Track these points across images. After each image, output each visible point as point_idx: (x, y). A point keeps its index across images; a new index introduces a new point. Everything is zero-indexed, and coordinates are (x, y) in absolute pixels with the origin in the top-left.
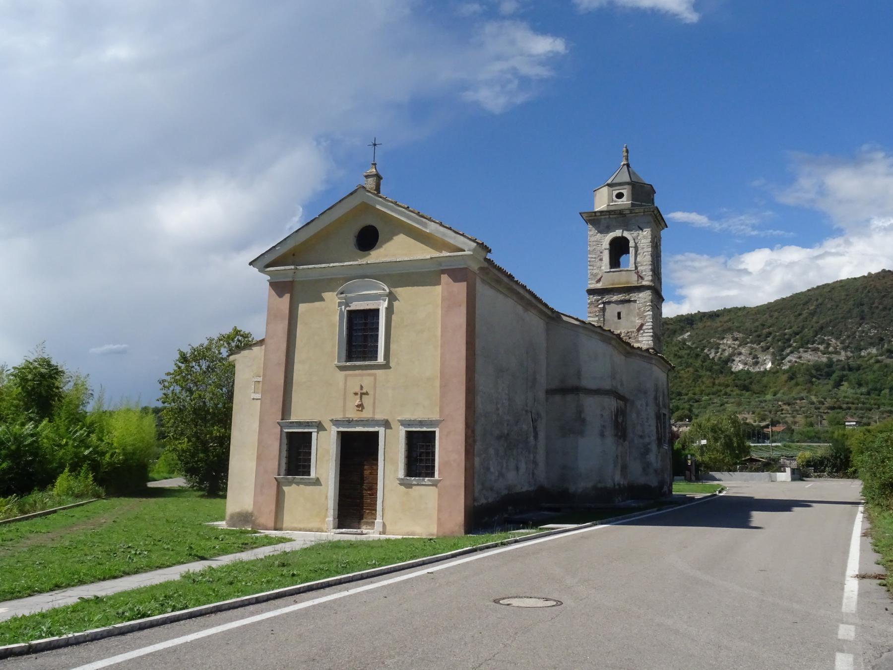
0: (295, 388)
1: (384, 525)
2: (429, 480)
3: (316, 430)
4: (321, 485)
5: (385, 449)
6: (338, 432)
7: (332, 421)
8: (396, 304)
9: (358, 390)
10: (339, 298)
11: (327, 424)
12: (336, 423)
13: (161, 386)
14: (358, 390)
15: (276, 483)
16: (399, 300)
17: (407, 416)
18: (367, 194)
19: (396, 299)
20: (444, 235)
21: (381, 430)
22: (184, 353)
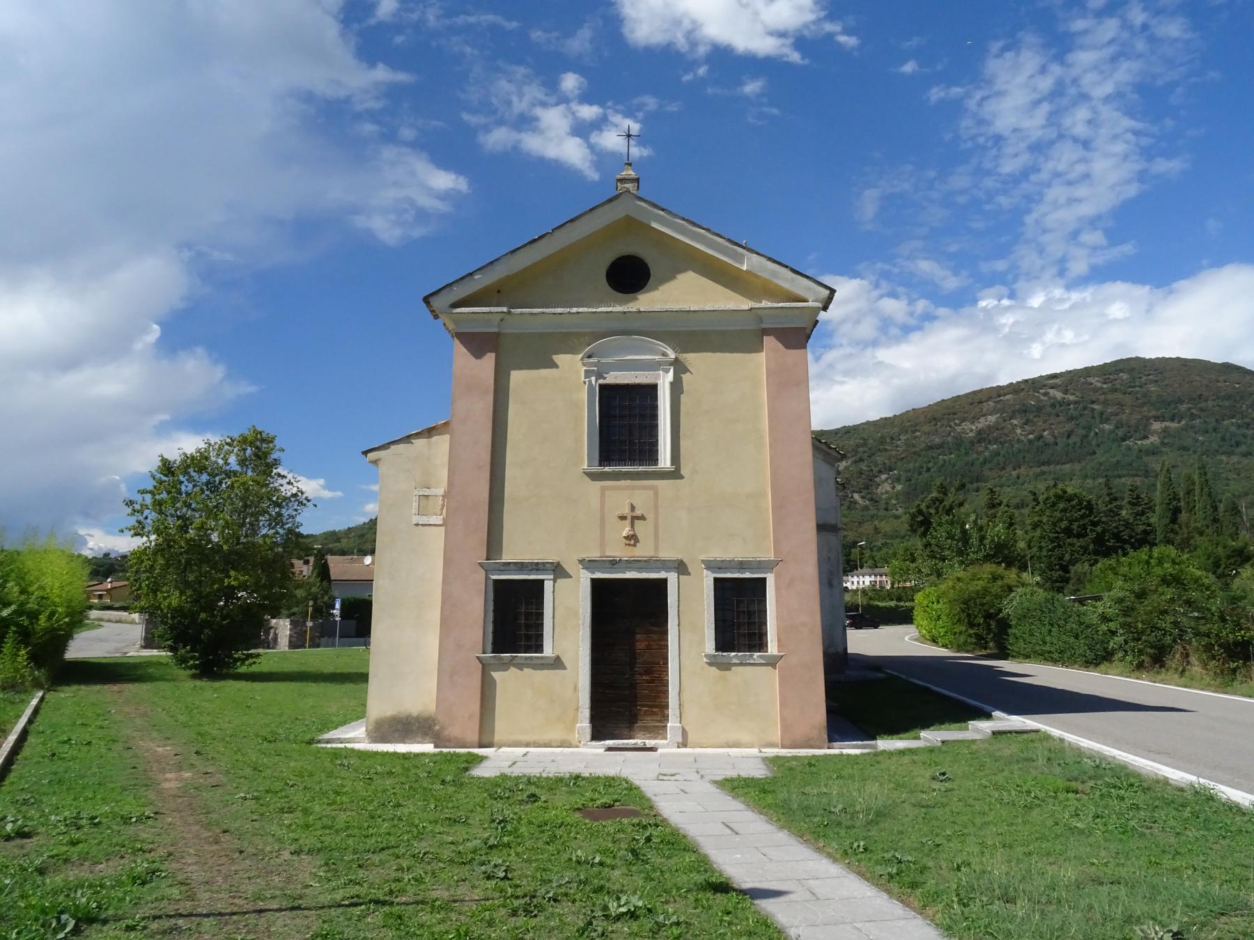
0: (507, 507)
1: (684, 733)
2: (761, 657)
3: (552, 577)
4: (565, 668)
5: (678, 607)
6: (594, 581)
7: (581, 561)
8: (686, 377)
9: (626, 511)
10: (584, 364)
11: (570, 566)
12: (588, 564)
13: (129, 510)
14: (626, 511)
15: (481, 666)
16: (690, 371)
17: (717, 554)
18: (639, 203)
19: (686, 370)
20: (775, 274)
21: (672, 578)
22: (170, 462)
